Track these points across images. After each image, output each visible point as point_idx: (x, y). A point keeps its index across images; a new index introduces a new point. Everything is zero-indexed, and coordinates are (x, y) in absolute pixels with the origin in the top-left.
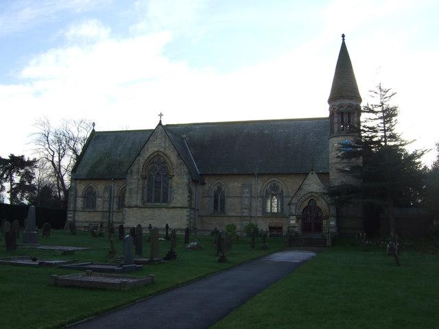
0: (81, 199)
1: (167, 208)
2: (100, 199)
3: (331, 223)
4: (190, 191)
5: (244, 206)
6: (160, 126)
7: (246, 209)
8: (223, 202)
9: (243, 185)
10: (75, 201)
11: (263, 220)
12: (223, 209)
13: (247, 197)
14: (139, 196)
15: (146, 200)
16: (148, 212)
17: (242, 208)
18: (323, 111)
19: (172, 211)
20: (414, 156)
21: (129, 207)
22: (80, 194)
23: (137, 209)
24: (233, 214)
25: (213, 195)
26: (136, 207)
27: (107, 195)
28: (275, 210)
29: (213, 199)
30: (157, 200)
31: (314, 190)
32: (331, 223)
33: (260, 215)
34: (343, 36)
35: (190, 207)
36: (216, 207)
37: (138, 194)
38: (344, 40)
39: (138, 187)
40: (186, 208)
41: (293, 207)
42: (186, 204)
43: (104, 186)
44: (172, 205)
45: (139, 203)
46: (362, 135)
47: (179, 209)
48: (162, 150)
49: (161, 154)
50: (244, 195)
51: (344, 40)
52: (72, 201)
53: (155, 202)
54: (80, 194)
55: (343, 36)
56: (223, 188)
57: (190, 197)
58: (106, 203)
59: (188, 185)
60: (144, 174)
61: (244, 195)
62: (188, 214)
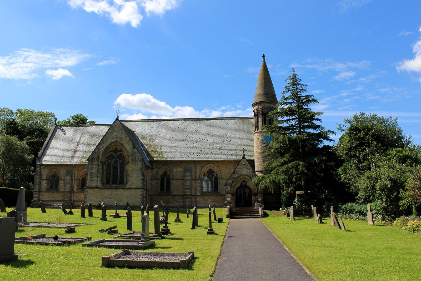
0: (45, 182)
1: (123, 189)
2: (62, 182)
3: (259, 199)
4: (143, 175)
5: (186, 187)
6: (117, 121)
7: (187, 189)
8: (168, 183)
9: (185, 169)
10: (40, 184)
11: (201, 198)
12: (168, 190)
13: (189, 180)
14: (99, 179)
15: (105, 182)
16: (107, 192)
17: (184, 189)
18: (179, 214)
19: (128, 191)
20: (107, 216)
21: (91, 188)
22: (44, 177)
23: (97, 190)
24: (177, 193)
25: (160, 178)
26: (96, 188)
27: (68, 178)
28: (209, 191)
29: (160, 181)
30: (115, 182)
31: (245, 173)
32: (259, 199)
33: (200, 194)
34: (264, 56)
35: (143, 188)
36: (162, 190)
37: (98, 177)
38: (264, 59)
39: (98, 172)
40: (140, 188)
41: (229, 187)
42: (140, 185)
43: (65, 171)
44: (128, 186)
45: (99, 185)
46: (298, 116)
47: (134, 190)
48: (119, 140)
49: (118, 144)
50: (186, 178)
51: (264, 59)
52: (37, 183)
53: (113, 184)
54: (44, 177)
55: (264, 56)
56: (168, 173)
57: (143, 179)
58: (68, 185)
59: (142, 169)
60: (103, 160)
61: (186, 178)
62: (142, 193)
